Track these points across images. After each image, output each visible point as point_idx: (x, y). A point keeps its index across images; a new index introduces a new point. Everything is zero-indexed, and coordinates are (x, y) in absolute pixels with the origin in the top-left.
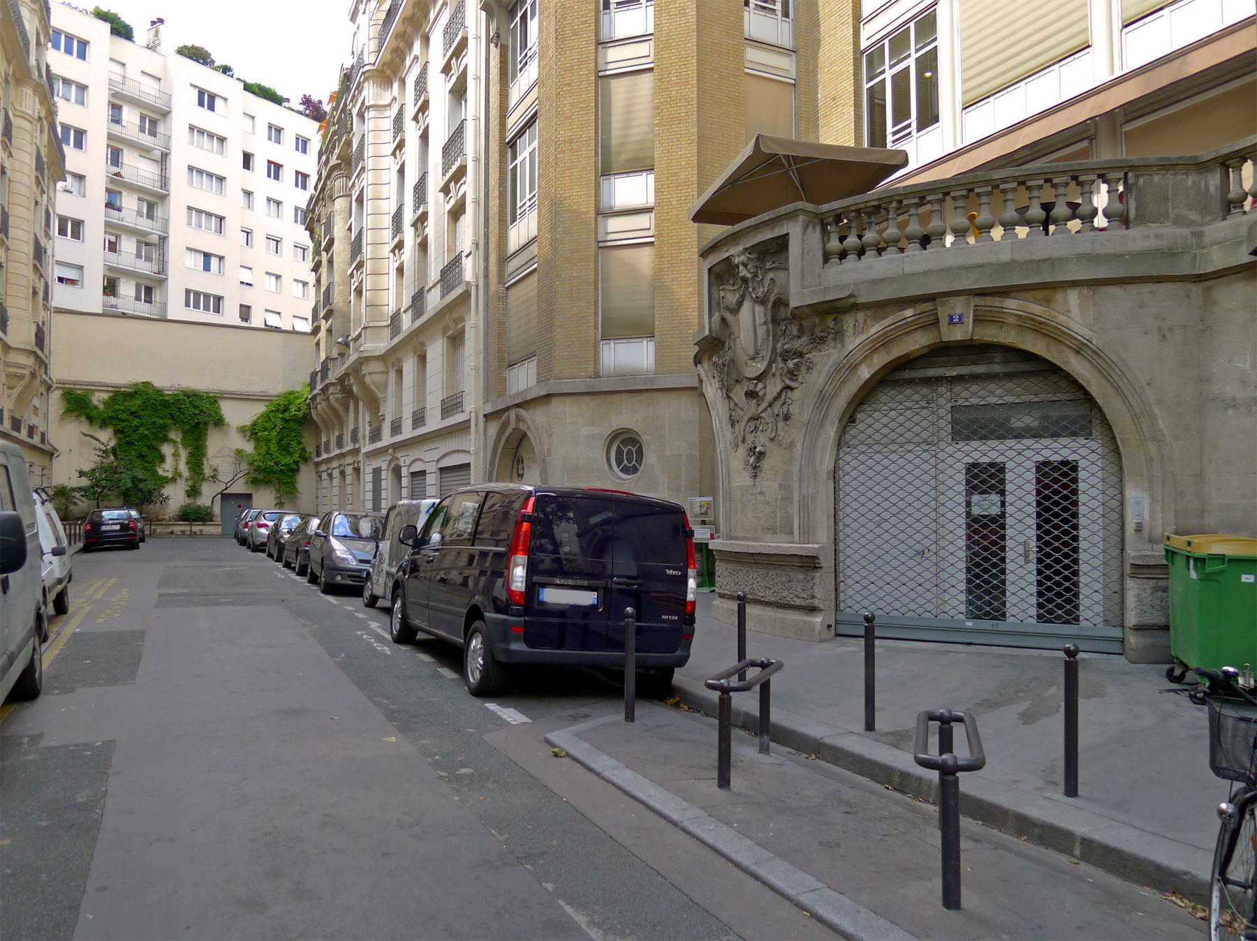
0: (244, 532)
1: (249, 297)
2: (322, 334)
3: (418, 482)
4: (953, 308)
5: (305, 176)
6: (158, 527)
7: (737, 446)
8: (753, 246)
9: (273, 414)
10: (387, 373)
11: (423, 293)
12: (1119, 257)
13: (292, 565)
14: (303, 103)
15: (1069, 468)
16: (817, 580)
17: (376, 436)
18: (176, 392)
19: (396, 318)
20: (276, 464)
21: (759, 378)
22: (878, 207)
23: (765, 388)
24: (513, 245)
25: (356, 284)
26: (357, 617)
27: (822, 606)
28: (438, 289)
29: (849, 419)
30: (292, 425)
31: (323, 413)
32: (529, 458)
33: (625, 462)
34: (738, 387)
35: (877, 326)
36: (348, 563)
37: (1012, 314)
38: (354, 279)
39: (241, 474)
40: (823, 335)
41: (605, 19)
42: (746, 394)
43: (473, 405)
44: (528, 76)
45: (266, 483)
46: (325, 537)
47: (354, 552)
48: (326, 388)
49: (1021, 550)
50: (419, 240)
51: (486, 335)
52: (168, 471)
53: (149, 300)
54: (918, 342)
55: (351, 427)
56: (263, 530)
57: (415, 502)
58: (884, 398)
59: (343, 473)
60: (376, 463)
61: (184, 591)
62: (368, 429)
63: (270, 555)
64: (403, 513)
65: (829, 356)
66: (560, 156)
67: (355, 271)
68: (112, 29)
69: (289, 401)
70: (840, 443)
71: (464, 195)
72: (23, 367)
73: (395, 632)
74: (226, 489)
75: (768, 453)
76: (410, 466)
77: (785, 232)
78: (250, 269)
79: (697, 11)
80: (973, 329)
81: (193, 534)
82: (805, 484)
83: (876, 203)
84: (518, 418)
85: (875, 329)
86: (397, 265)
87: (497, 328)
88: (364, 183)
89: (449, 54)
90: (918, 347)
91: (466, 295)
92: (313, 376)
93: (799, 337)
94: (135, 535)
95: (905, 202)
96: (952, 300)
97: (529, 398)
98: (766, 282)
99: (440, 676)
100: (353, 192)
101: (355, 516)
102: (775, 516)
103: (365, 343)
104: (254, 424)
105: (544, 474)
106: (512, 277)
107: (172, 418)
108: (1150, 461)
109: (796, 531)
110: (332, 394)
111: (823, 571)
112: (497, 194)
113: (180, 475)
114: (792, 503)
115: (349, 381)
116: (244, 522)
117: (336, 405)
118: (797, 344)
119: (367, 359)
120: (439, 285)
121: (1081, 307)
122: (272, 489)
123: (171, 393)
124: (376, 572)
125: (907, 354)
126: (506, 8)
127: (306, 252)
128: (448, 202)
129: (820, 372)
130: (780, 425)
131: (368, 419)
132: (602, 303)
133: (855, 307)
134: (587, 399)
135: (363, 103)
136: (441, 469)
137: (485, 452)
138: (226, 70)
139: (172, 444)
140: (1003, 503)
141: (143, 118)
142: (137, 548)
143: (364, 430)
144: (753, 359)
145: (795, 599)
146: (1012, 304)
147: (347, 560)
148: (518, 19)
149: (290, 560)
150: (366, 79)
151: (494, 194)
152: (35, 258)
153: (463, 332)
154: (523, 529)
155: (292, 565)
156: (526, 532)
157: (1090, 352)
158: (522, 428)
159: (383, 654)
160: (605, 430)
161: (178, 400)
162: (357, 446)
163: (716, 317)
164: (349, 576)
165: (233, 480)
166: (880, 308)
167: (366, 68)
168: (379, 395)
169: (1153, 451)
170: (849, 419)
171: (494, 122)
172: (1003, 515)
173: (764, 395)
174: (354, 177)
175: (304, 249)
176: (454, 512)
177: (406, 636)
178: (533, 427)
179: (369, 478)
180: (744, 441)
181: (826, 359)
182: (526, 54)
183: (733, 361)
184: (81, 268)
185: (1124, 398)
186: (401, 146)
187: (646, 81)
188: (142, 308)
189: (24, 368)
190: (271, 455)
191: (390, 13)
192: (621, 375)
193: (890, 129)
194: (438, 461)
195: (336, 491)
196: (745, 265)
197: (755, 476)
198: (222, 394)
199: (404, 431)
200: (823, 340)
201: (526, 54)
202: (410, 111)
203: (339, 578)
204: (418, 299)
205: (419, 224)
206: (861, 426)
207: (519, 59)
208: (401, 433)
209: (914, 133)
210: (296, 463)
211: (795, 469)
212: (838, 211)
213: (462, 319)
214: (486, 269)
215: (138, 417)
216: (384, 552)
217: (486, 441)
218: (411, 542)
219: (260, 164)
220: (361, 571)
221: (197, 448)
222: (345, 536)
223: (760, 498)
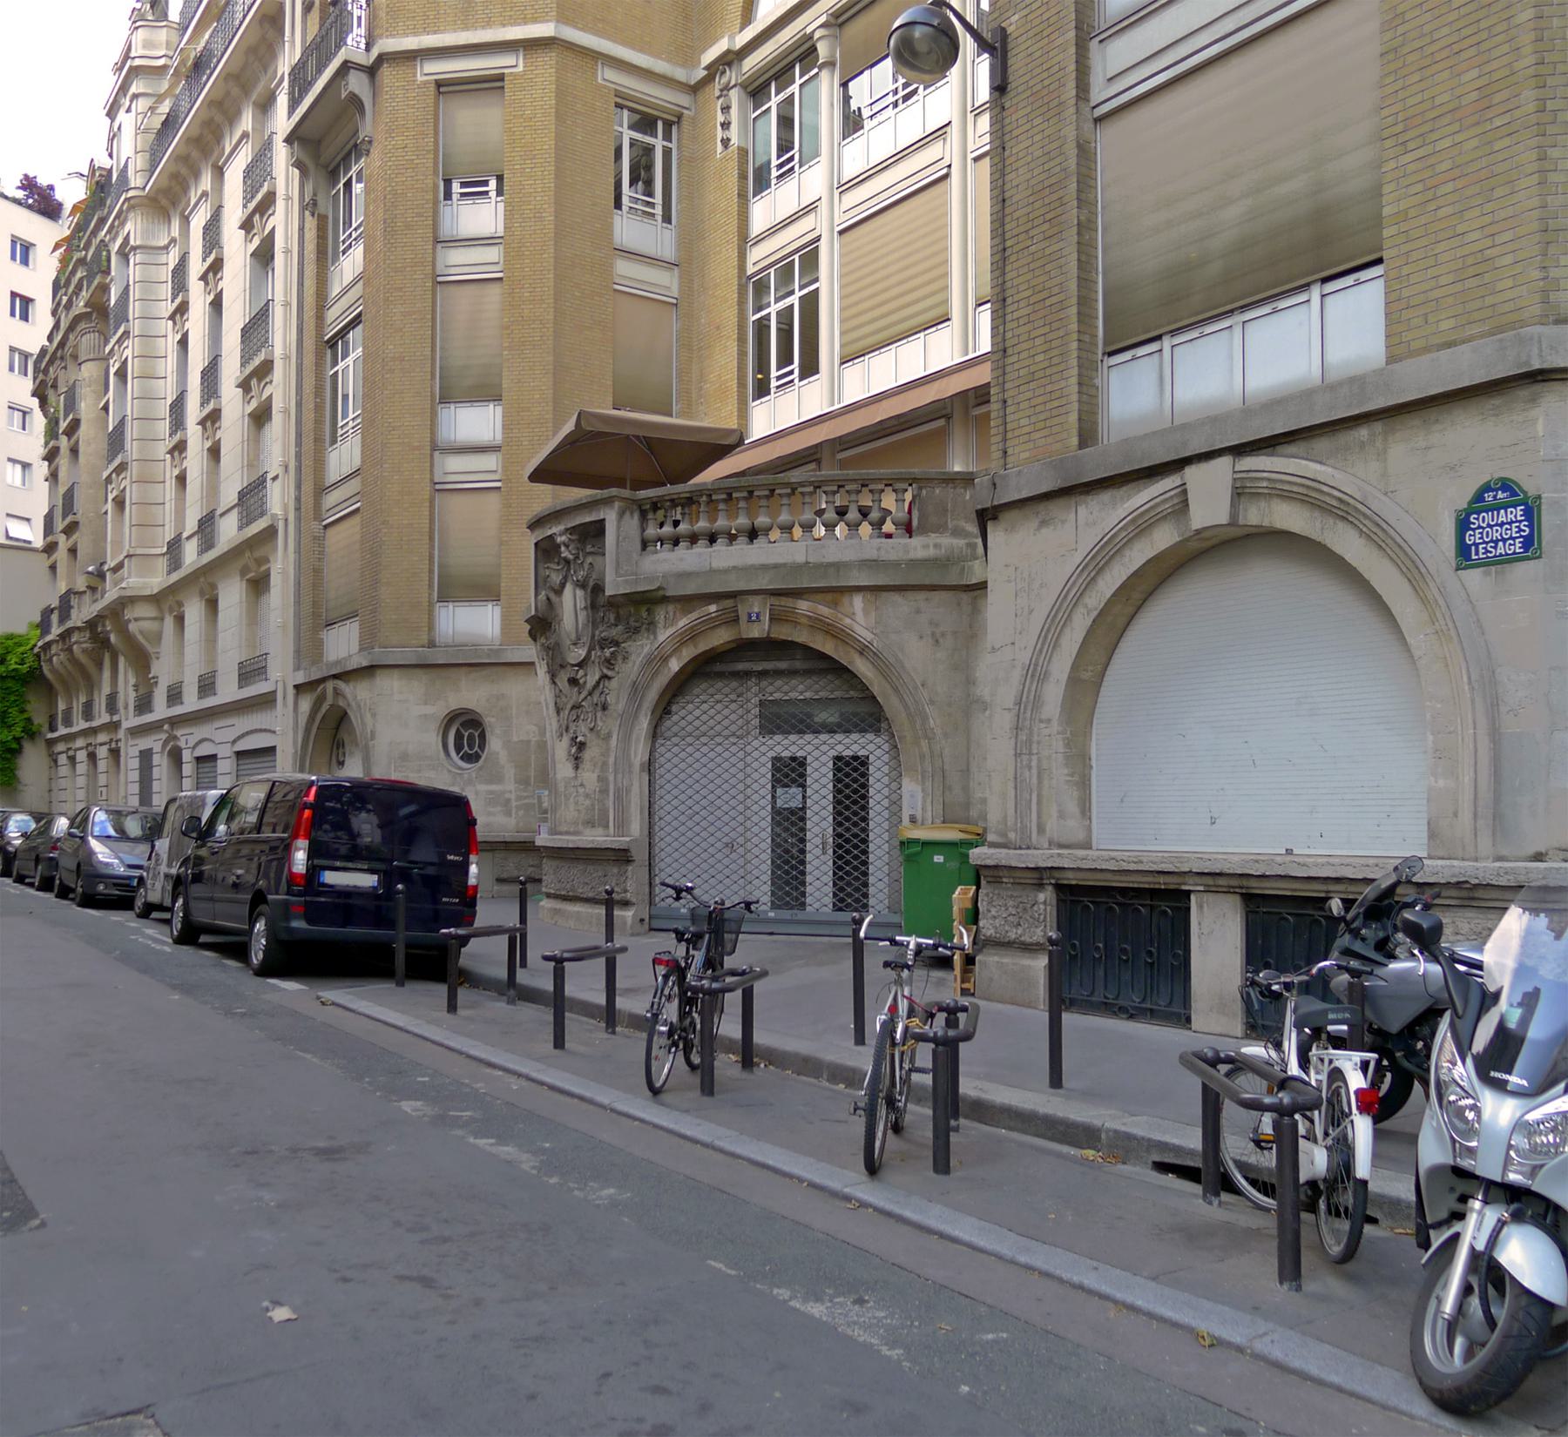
2: (61, 554)
3: (206, 770)
4: (751, 606)
5: (27, 302)
7: (562, 735)
8: (573, 527)
10: (162, 619)
12: (895, 565)
14: (23, 187)
15: (863, 762)
16: (629, 874)
17: (144, 705)
19: (175, 546)
21: (581, 665)
22: (690, 499)
23: (586, 675)
24: (333, 475)
27: (634, 900)
29: (664, 710)
31: (62, 671)
33: (466, 748)
34: (562, 672)
35: (684, 619)
36: (114, 869)
37: (803, 615)
38: (113, 486)
40: (637, 625)
41: (446, 211)
42: (569, 680)
43: (282, 673)
44: (351, 264)
46: (81, 838)
47: (121, 855)
48: (65, 636)
49: (818, 841)
50: (208, 444)
51: (298, 584)
54: (720, 638)
57: (199, 793)
58: (696, 691)
59: (92, 757)
60: (145, 743)
62: (132, 695)
65: (642, 646)
66: (388, 376)
67: (114, 475)
69: (7, 648)
70: (655, 734)
71: (270, 397)
73: (175, 933)
75: (588, 745)
76: (194, 748)
77: (602, 517)
79: (556, 217)
80: (770, 626)
82: (620, 776)
83: (688, 495)
84: (337, 692)
85: (683, 622)
86: (176, 472)
87: (312, 577)
88: (128, 352)
89: (252, 206)
90: (722, 642)
91: (270, 533)
92: (47, 612)
93: (616, 625)
95: (714, 497)
96: (751, 598)
98: (586, 566)
99: (224, 966)
100: (112, 362)
102: (594, 809)
103: (130, 576)
105: (367, 761)
106: (331, 513)
108: (922, 757)
109: (611, 824)
110: (76, 643)
111: (635, 864)
112: (312, 406)
114: (608, 795)
115: (104, 626)
117: (83, 659)
118: (614, 632)
119: (132, 600)
121: (866, 612)
124: (150, 875)
125: (713, 648)
126: (327, 167)
127: (27, 417)
128: (249, 402)
129: (634, 662)
130: (599, 714)
131: (132, 681)
132: (439, 556)
133: (665, 600)
134: (419, 671)
135: (127, 239)
136: (240, 755)
140: (804, 797)
143: (126, 695)
144: (575, 644)
146: (803, 606)
148: (341, 185)
149: (25, 873)
150: (131, 208)
151: (309, 405)
153: (267, 575)
156: (307, 818)
157: (871, 654)
158: (341, 704)
159: (164, 953)
160: (440, 710)
162: (115, 718)
163: (542, 596)
164: (115, 885)
166: (688, 602)
167: (131, 194)
169: (925, 749)
170: (664, 710)
171: (310, 313)
172: (803, 809)
173: (585, 682)
174: (113, 341)
175: (25, 413)
176: (241, 801)
177: (189, 935)
178: (353, 704)
180: (567, 729)
181: (641, 649)
182: (351, 234)
183: (557, 644)
185: (902, 699)
187: (495, 291)
191: (170, 124)
192: (459, 646)
193: (774, 373)
194: (234, 742)
195: (81, 781)
196: (567, 546)
197: (577, 768)
200: (637, 631)
201: (351, 234)
203: (101, 887)
204: (207, 524)
205: (211, 275)
206: (675, 718)
207: (342, 238)
209: (796, 381)
210: (18, 740)
211: (611, 760)
212: (654, 500)
214: (298, 499)
216: (161, 852)
218: (194, 835)
220: (130, 878)
223: (581, 790)
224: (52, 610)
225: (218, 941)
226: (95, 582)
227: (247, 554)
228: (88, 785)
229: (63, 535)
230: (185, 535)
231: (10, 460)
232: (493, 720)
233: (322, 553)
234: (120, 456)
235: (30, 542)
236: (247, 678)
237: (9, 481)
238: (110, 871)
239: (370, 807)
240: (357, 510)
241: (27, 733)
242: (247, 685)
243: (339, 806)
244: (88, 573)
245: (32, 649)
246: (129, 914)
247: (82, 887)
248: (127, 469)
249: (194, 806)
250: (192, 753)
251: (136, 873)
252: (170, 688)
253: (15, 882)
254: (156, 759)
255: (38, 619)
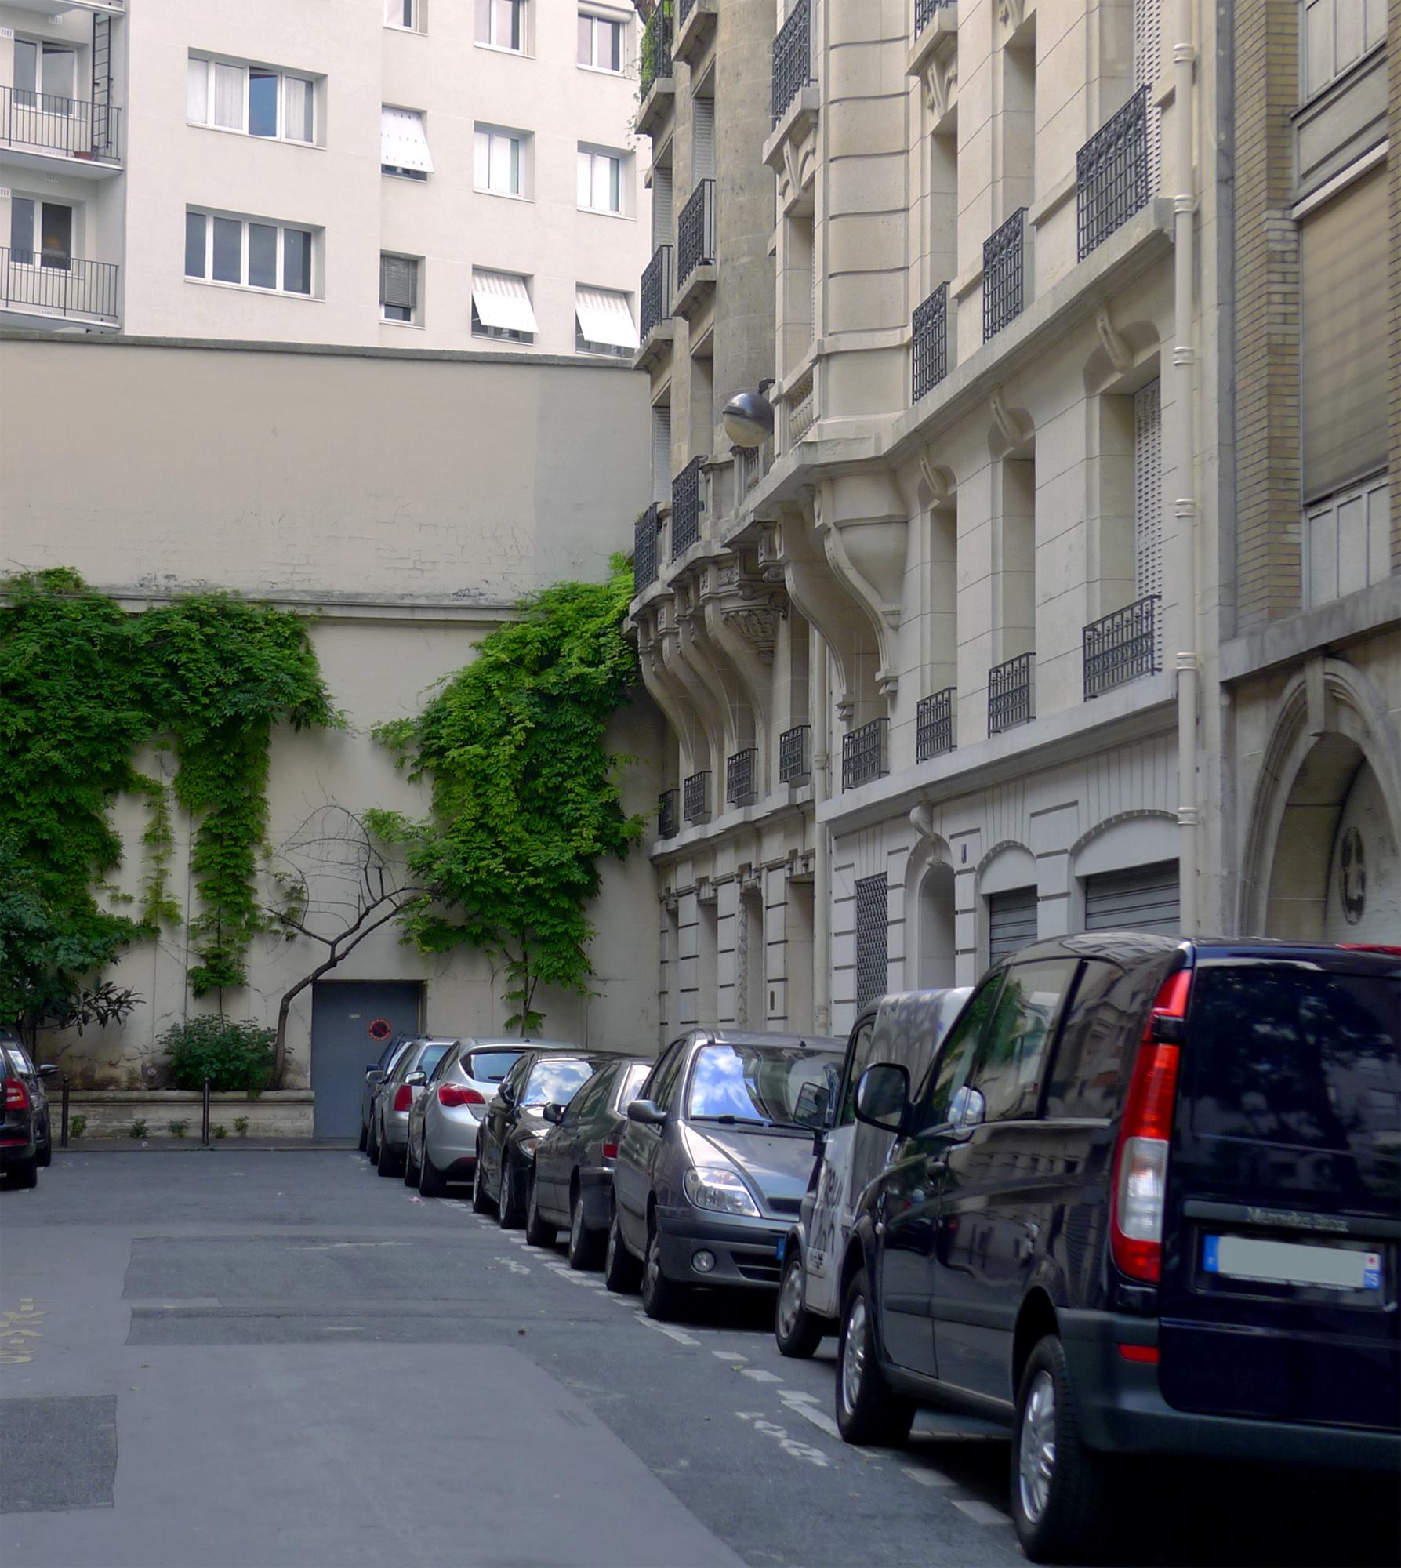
0: (397, 1125)
2: (680, 369)
6: (92, 1111)
9: (501, 677)
10: (905, 522)
11: (1019, 232)
13: (561, 1237)
18: (159, 606)
20: (510, 865)
25: (791, 195)
26: (749, 1380)
30: (569, 714)
31: (683, 675)
32: (1382, 840)
38: (787, 176)
39: (387, 908)
45: (477, 940)
46: (661, 1122)
50: (1007, 33)
51: (1230, 392)
52: (128, 899)
53: (58, 260)
55: (783, 721)
56: (464, 1117)
59: (752, 900)
60: (869, 861)
61: (211, 1303)
62: (840, 729)
63: (486, 1207)
64: (894, 1031)
67: (787, 148)
69: (560, 624)
74: (333, 963)
78: (419, 114)
81: (211, 1138)
84: (1336, 697)
86: (934, 121)
92: (650, 523)
94: (23, 1135)
97: (1365, 623)
99: (957, 1517)
101: (772, 1053)
103: (825, 413)
104: (435, 718)
107: (145, 699)
113: (170, 915)
115: (771, 550)
116: (394, 1086)
117: (729, 642)
120: (1072, 208)
122: (499, 962)
123: (140, 608)
127: (623, 34)
131: (839, 693)
136: (1094, 885)
137: (1229, 817)
139: (144, 800)
142: (30, 1182)
143: (827, 733)
147: (732, 1201)
149: (552, 1216)
153: (1150, 381)
154: (1158, 1064)
155: (561, 1237)
161: (167, 635)
162: (802, 795)
164: (738, 1256)
165: (358, 931)
168: (878, 605)
178: (1378, 729)
179: (845, 916)
190: (492, 831)
194: (1077, 851)
195: (728, 967)
198: (319, 605)
199: (1040, 712)
203: (703, 1263)
208: (952, 747)
210: (585, 861)
213: (1149, 335)
214: (1226, 153)
215: (28, 700)
217: (1233, 775)
218: (895, 1119)
221: (229, 811)
222: (728, 1120)
224: (659, 521)
225: (967, 1435)
226: (749, 434)
227: (1101, 322)
228: (743, 977)
229: (680, 319)
230: (955, 288)
231: (481, 127)
233: (1293, 298)
234: (798, 96)
235: (527, 337)
236: (1105, 669)
237: (480, 183)
238: (724, 1218)
239: (1387, 1039)
240: (1379, 167)
241: (607, 844)
242: (1105, 690)
243: (1289, 1034)
244: (733, 412)
245: (619, 622)
246: (764, 1344)
247: (657, 1261)
248: (816, 125)
249: (914, 1033)
250: (977, 884)
251: (782, 1223)
252: (925, 707)
253: (531, 1242)
254: (895, 904)
255: (627, 543)
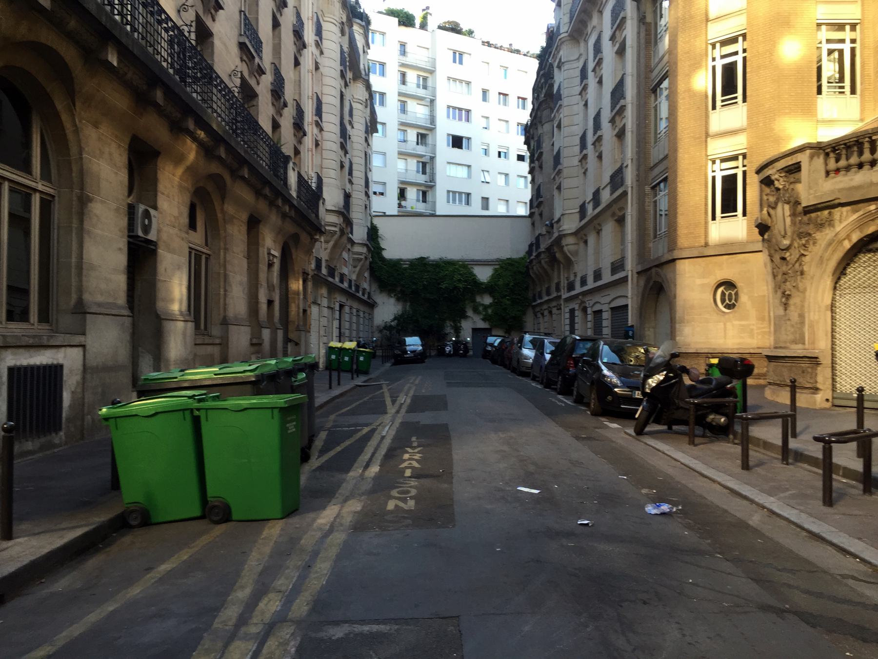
1: (486, 192)
5: (524, 99)
28: (608, 188)
43: (631, 265)
60: (572, 305)
68: (399, 22)
72: (361, 254)
75: (792, 295)
83: (855, 139)
84: (658, 274)
88: (561, 115)
92: (531, 246)
109: (807, 342)
117: (546, 266)
120: (609, 186)
136: (612, 309)
138: (470, 33)
141: (419, 76)
143: (564, 283)
145: (807, 384)
152: (366, 187)
162: (559, 294)
168: (573, 259)
179: (567, 315)
181: (824, 237)
184: (384, 184)
186: (585, 88)
188: (421, 207)
189: (361, 255)
194: (610, 303)
197: (786, 309)
199: (588, 283)
202: (591, 65)
212: (834, 145)
219: (493, 96)
232: (742, 284)
